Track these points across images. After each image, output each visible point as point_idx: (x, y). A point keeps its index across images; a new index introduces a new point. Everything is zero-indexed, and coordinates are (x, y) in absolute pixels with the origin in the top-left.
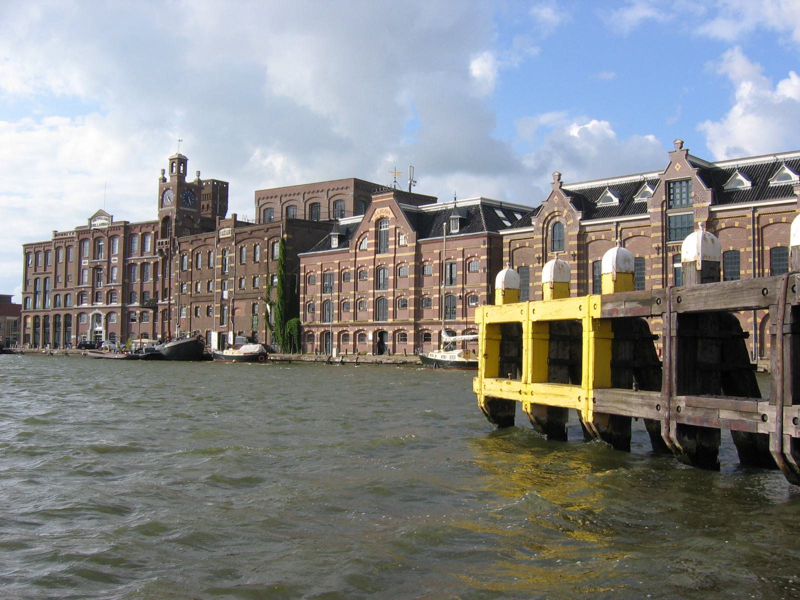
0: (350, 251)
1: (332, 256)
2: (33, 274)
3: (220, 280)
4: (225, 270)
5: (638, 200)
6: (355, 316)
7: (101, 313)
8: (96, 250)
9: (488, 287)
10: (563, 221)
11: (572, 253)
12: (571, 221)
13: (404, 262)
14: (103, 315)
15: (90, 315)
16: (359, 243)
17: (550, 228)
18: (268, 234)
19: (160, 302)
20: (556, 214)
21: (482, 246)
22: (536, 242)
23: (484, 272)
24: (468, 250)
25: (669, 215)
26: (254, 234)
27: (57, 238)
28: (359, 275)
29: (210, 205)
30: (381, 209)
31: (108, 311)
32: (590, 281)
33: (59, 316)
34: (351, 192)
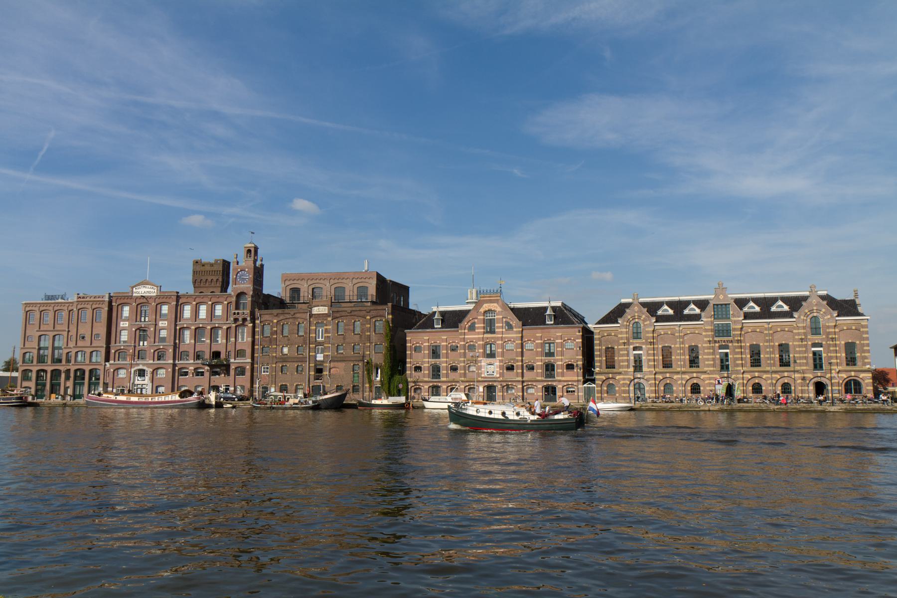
0: (460, 331)
2: (37, 331)
3: (314, 346)
6: (465, 375)
8: (138, 313)
10: (641, 322)
14: (149, 370)
15: (133, 370)
18: (370, 314)
20: (636, 317)
21: (578, 334)
22: (621, 333)
23: (580, 349)
26: (353, 313)
27: (80, 300)
30: (489, 304)
31: (156, 367)
32: (661, 358)
33: (45, 371)
34: (374, 282)
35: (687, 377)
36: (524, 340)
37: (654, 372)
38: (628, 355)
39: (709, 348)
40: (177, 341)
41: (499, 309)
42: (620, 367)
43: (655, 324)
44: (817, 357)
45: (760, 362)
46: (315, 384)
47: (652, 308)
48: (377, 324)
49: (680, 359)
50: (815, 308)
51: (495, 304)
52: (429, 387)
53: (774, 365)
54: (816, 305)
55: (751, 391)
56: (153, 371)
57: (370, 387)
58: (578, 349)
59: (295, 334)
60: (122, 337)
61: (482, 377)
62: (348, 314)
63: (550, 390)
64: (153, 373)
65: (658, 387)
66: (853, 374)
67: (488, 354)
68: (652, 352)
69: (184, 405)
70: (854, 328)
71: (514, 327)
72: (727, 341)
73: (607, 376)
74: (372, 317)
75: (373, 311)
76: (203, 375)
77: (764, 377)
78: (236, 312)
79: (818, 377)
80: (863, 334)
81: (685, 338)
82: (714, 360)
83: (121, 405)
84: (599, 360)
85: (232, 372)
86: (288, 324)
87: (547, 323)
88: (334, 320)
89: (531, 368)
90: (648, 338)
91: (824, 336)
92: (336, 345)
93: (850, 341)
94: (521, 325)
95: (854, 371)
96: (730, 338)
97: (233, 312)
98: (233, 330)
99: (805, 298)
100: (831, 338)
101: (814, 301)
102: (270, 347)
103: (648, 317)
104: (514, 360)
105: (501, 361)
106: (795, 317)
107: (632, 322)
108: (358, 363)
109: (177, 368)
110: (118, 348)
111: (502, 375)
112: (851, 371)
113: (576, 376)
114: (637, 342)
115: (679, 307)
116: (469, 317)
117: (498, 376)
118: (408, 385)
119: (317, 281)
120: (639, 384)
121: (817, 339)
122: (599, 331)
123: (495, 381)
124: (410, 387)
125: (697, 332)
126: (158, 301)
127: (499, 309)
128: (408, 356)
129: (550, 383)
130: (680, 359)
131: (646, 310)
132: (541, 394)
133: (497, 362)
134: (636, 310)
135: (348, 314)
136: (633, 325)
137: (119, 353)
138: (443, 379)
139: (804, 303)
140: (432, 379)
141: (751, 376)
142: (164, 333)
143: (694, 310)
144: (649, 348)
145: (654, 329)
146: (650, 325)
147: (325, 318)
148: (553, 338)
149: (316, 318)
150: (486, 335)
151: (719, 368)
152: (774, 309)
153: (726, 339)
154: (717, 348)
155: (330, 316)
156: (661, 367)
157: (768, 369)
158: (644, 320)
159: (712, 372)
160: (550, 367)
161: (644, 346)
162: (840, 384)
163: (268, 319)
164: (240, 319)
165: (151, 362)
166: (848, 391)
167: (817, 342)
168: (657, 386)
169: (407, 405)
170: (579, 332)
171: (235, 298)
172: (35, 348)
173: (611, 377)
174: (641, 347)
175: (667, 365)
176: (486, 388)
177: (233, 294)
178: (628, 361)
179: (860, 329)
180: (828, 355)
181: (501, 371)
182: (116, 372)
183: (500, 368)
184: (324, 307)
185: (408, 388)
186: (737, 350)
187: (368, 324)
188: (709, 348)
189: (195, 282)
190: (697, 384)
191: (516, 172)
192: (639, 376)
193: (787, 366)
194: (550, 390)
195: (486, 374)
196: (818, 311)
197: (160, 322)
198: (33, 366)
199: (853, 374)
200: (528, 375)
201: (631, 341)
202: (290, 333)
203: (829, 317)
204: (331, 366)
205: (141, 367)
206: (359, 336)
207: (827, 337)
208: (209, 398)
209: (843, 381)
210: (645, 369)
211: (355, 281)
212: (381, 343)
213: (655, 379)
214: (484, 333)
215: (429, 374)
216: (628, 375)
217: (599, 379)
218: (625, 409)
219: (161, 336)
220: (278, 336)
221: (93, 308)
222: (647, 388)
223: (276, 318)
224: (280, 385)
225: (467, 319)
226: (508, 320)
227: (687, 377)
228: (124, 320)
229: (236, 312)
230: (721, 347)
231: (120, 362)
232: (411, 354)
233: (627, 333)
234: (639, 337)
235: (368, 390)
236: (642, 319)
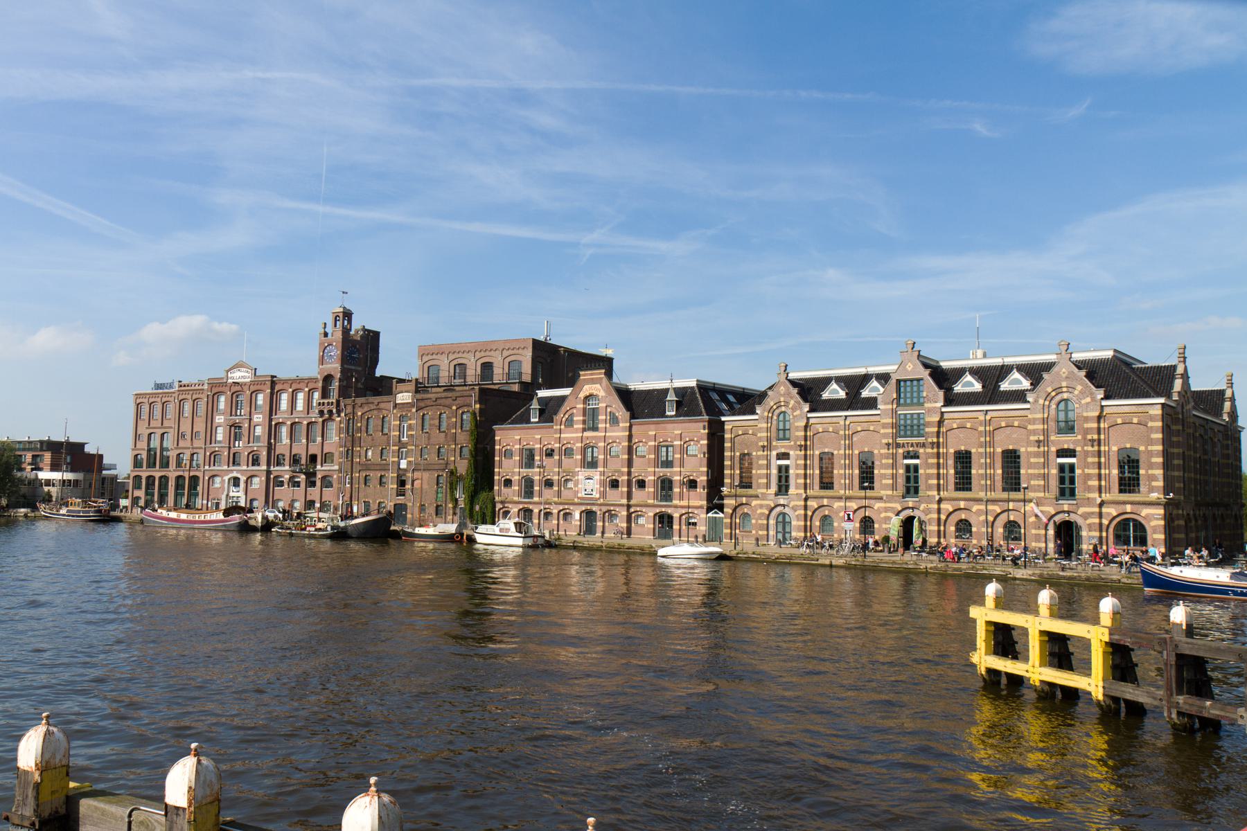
2: (147, 428)
3: (397, 448)
5: (865, 393)
7: (239, 475)
8: (234, 405)
9: (708, 472)
10: (789, 411)
11: (799, 443)
12: (798, 412)
14: (243, 479)
15: (226, 478)
16: (564, 419)
17: (775, 418)
18: (456, 402)
19: (319, 467)
20: (1065, 390)
21: (702, 431)
22: (1034, 421)
23: (704, 456)
25: (899, 412)
26: (439, 402)
28: (568, 452)
31: (249, 474)
32: (817, 472)
35: (997, 509)
36: (633, 442)
37: (937, 498)
38: (768, 467)
39: (1036, 455)
40: (272, 441)
41: (602, 393)
42: (759, 486)
43: (809, 415)
44: (1067, 475)
45: (970, 483)
46: (398, 502)
47: (809, 391)
48: (465, 417)
49: (844, 474)
50: (1064, 384)
51: (598, 386)
52: (519, 510)
53: (993, 488)
54: (1067, 377)
55: (953, 534)
56: (247, 479)
57: (455, 508)
58: (702, 456)
60: (218, 435)
61: (578, 498)
62: (434, 403)
63: (666, 520)
64: (246, 482)
65: (945, 526)
66: (1128, 508)
67: (588, 463)
68: (935, 461)
69: (225, 526)
70: (1135, 420)
71: (620, 421)
72: (917, 444)
73: (1005, 506)
76: (299, 486)
77: (975, 508)
78: (322, 401)
79: (1064, 512)
80: (1152, 432)
81: (855, 439)
82: (1045, 477)
83: (171, 524)
84: (731, 474)
85: (318, 483)
87: (668, 413)
89: (641, 484)
90: (1087, 431)
91: (1079, 437)
93: (1128, 446)
94: (628, 418)
95: (1132, 503)
96: (921, 440)
98: (319, 428)
99: (1048, 367)
100: (1090, 440)
101: (1064, 370)
103: (799, 403)
104: (619, 471)
105: (603, 474)
106: (1029, 402)
107: (777, 412)
109: (272, 476)
110: (213, 450)
111: (603, 494)
112: (1125, 503)
113: (698, 499)
114: (781, 447)
115: (991, 377)
116: (566, 407)
117: (598, 496)
118: (494, 507)
119: (460, 355)
120: (784, 514)
121: (1067, 441)
122: (730, 427)
123: (593, 504)
124: (497, 509)
125: (872, 428)
126: (253, 388)
127: (602, 393)
128: (497, 464)
129: (663, 510)
130: (844, 474)
131: (796, 391)
132: (652, 526)
133: (596, 475)
134: (782, 392)
135: (434, 403)
136: (1058, 405)
137: (215, 456)
138: (676, 502)
139: (1045, 376)
140: (661, 501)
141: (953, 506)
142: (259, 431)
143: (1015, 382)
144: (797, 455)
145: (807, 423)
146: (800, 416)
148: (670, 437)
150: (587, 434)
151: (901, 490)
152: (1005, 386)
153: (915, 440)
154: (900, 457)
156: (817, 486)
157: (982, 495)
158: (794, 409)
159: (890, 499)
160: (667, 485)
161: (791, 453)
162: (1104, 528)
164: (326, 412)
165: (245, 468)
166: (1121, 539)
167: (1066, 447)
168: (809, 518)
169: (457, 537)
170: (704, 429)
171: (321, 382)
172: (144, 450)
173: (825, 504)
174: (788, 454)
175: (964, 482)
176: (584, 515)
177: (319, 377)
178: (768, 476)
179: (1147, 423)
180: (1083, 471)
181: (602, 489)
182: (211, 480)
183: (600, 484)
185: (495, 511)
186: (1090, 460)
188: (1036, 455)
190: (966, 520)
191: (980, 128)
192: (782, 502)
193: (967, 490)
194: (666, 520)
195: (584, 493)
196: (1070, 390)
197: (255, 416)
198: (156, 471)
199: (1128, 508)
200: (638, 496)
201: (774, 443)
202: (374, 431)
203: (1088, 400)
205: (235, 474)
207: (1085, 438)
208: (255, 518)
209: (1110, 522)
210: (792, 491)
211: (506, 353)
213: (1100, 515)
214: (584, 430)
215: (520, 491)
216: (767, 500)
217: (729, 506)
218: (708, 557)
219: (256, 434)
221: (194, 398)
222: (794, 523)
225: (563, 409)
226: (614, 411)
227: (997, 509)
228: (220, 414)
229: (326, 401)
230: (907, 456)
231: (216, 468)
232: (500, 461)
233: (1045, 421)
234: (787, 436)
235: (451, 512)
236: (790, 406)
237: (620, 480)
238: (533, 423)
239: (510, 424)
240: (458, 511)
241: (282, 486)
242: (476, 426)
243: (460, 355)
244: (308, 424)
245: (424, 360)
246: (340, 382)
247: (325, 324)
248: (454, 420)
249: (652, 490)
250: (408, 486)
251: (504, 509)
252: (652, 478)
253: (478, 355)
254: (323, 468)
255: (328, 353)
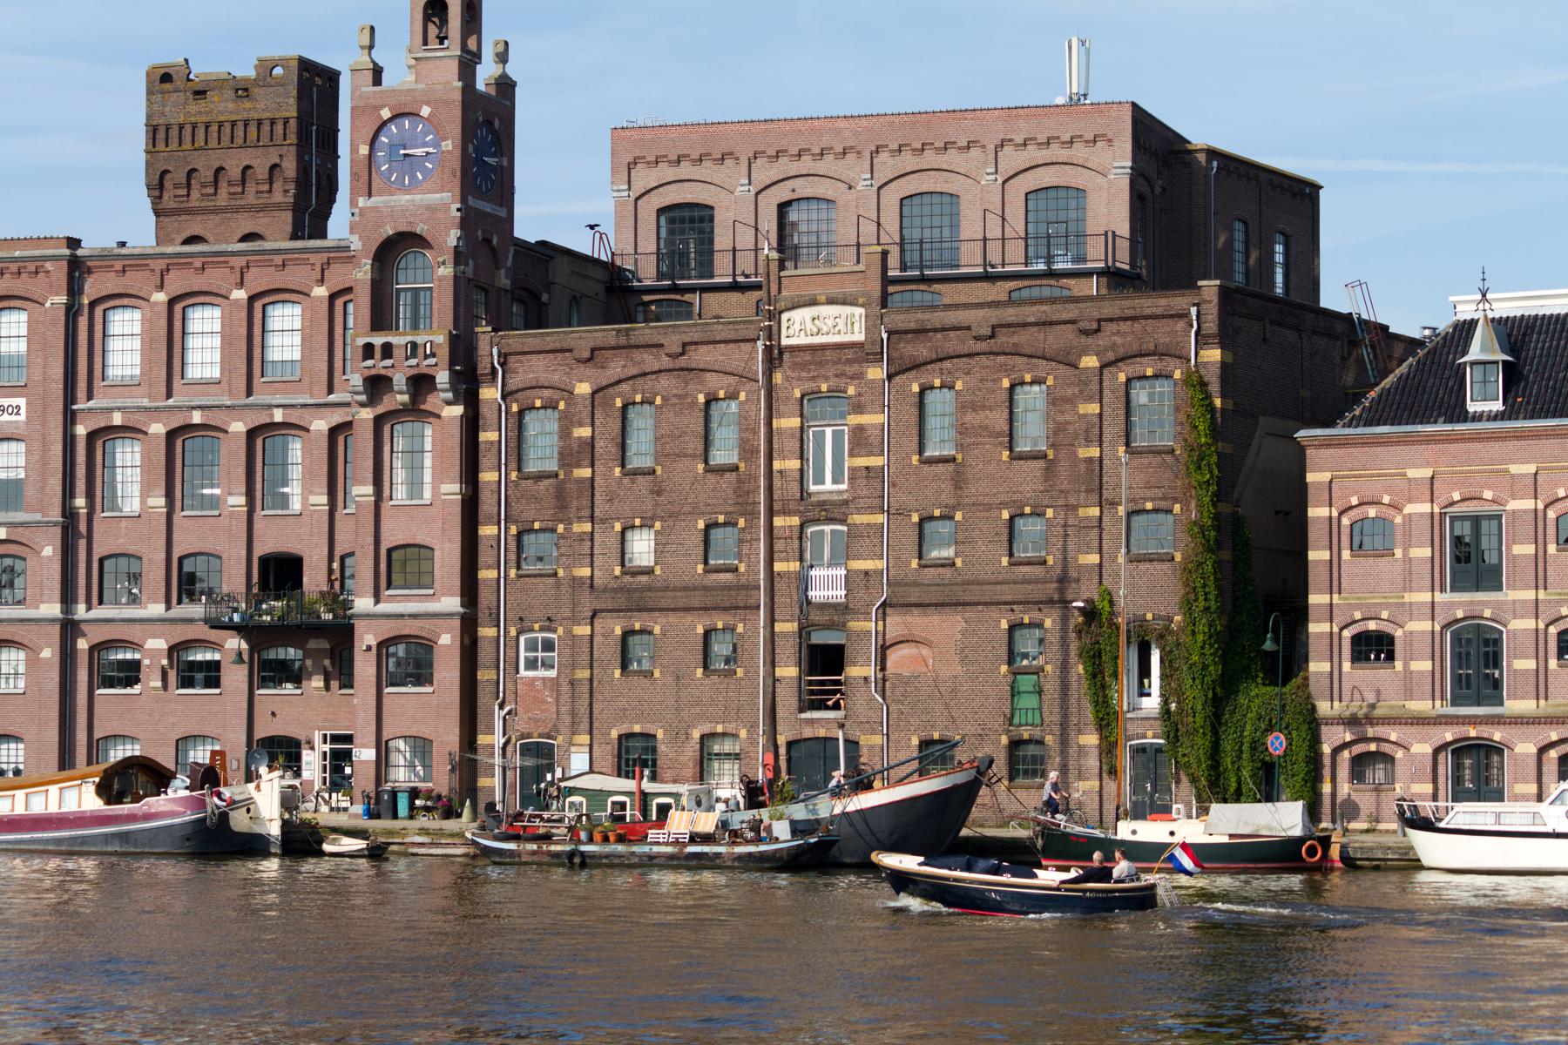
1: (1496, 446)
3: (795, 521)
4: (820, 480)
13: (1379, 503)
18: (1102, 340)
24: (1347, 483)
26: (1005, 340)
29: (290, 167)
34: (1118, 160)
40: (80, 502)
46: (808, 733)
48: (1141, 396)
57: (1108, 749)
59: (694, 456)
62: (980, 346)
74: (1110, 356)
75: (1113, 327)
85: (365, 668)
86: (651, 403)
88: (897, 379)
92: (915, 518)
97: (361, 341)
98: (362, 440)
102: (561, 528)
108: (1036, 615)
118: (1315, 741)
119: (806, 164)
124: (1326, 749)
128: (1316, 576)
135: (980, 346)
138: (1514, 706)
147: (851, 369)
149: (803, 366)
155: (876, 358)
163: (544, 378)
164: (399, 380)
169: (1312, 851)
171: (367, 264)
177: (356, 244)
184: (848, 310)
187: (1089, 399)
189: (157, 186)
204: (891, 635)
206: (1041, 463)
211: (1012, 159)
212: (1163, 504)
220: (599, 468)
223: (588, 371)
224: (614, 734)
232: (1333, 565)
235: (1093, 762)
237: (1398, 633)
238: (1478, 418)
239: (1353, 422)
240: (1125, 761)
241: (131, 681)
242: (1215, 432)
243: (806, 164)
244: (252, 434)
245: (640, 184)
246: (457, 263)
247: (372, 29)
248: (1094, 408)
249: (1426, 665)
250: (858, 670)
251: (1358, 749)
252: (1425, 626)
253: (887, 165)
254: (383, 607)
255: (393, 147)
